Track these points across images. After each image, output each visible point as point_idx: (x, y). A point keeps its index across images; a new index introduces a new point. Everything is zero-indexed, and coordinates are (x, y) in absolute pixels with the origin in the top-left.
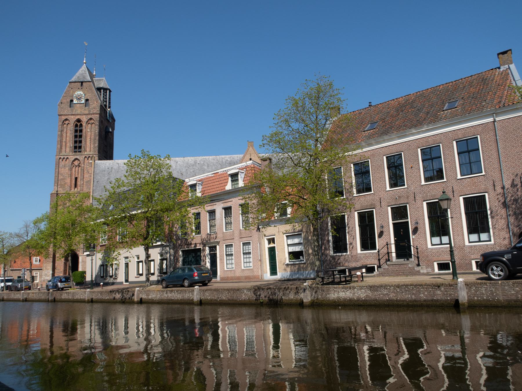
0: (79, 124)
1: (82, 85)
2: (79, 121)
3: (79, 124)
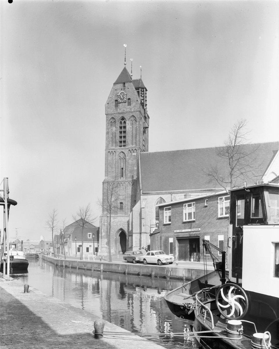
0: (123, 121)
1: (124, 86)
2: (123, 118)
3: (123, 121)
